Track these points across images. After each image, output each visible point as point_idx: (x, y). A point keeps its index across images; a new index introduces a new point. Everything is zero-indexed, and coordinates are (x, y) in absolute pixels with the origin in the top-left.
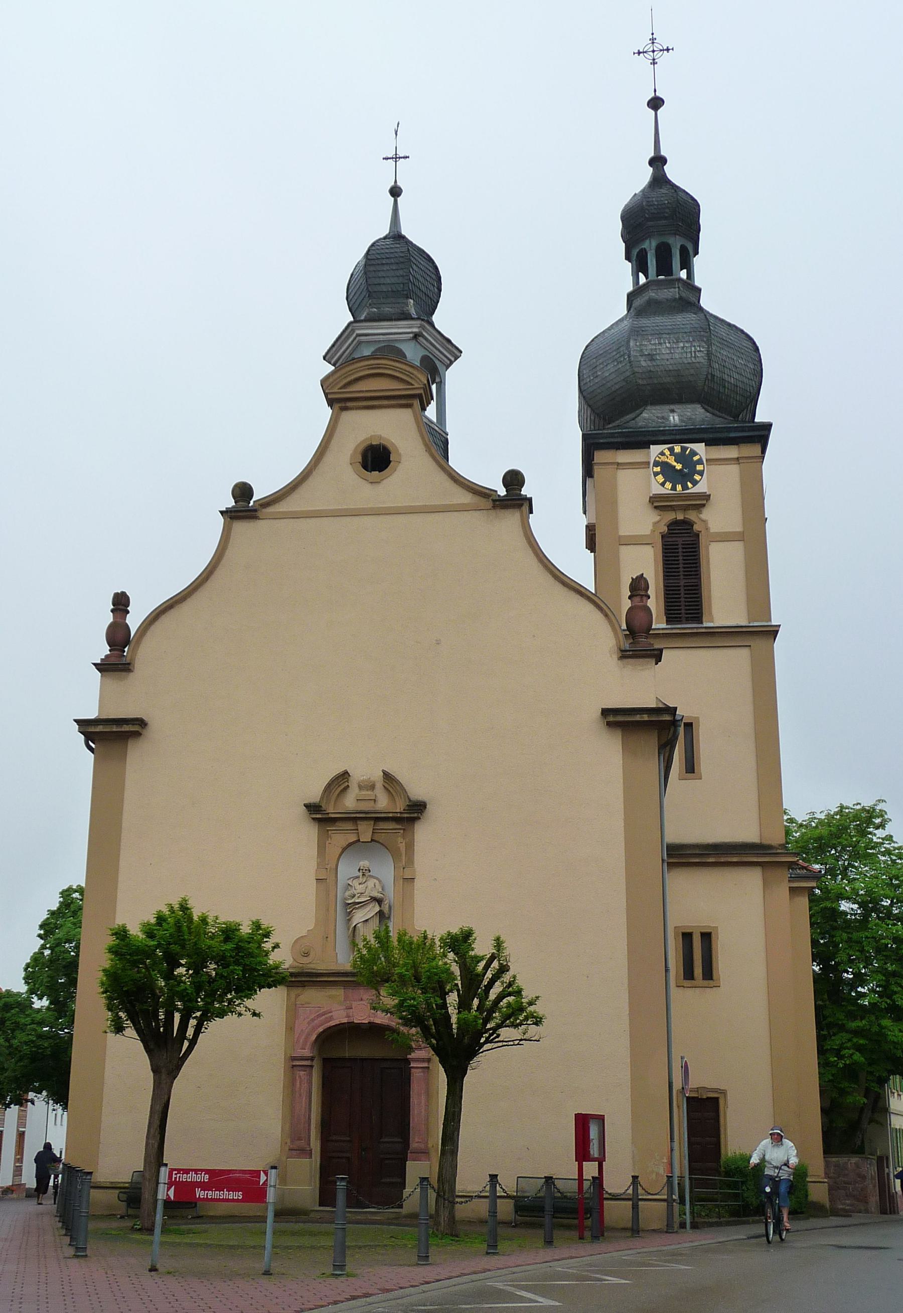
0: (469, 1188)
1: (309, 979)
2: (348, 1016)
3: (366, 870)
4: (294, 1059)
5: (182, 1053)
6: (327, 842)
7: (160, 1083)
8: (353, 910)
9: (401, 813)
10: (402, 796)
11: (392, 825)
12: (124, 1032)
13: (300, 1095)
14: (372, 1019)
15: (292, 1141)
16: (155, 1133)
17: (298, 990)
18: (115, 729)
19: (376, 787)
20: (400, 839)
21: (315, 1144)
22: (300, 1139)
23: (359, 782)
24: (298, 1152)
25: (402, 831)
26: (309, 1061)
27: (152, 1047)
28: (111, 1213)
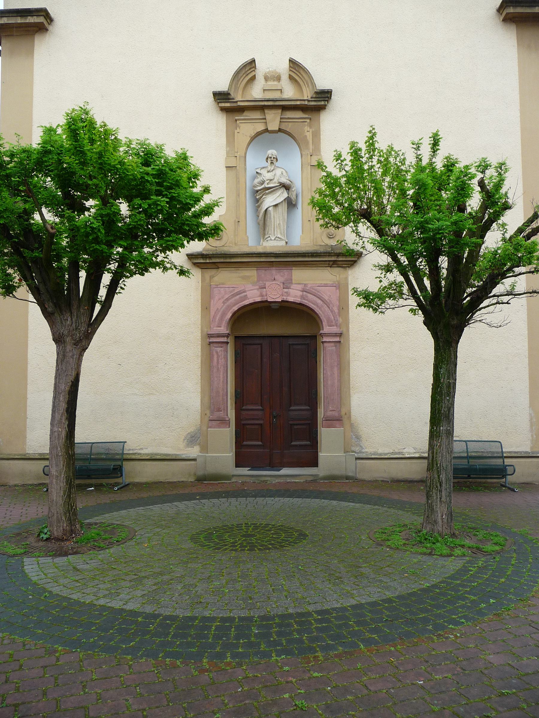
0: (380, 451)
1: (222, 260)
2: (261, 295)
3: (274, 158)
4: (210, 336)
5: (93, 319)
6: (236, 131)
7: (64, 356)
8: (263, 195)
9: (308, 101)
10: (310, 84)
11: (299, 114)
12: (14, 293)
13: (218, 369)
14: (285, 298)
15: (212, 412)
16: (61, 419)
17: (213, 272)
18: (19, 20)
19: (282, 79)
20: (307, 128)
21: (231, 414)
22: (219, 410)
23: (266, 73)
24: (218, 422)
25: (308, 121)
26: (226, 338)
27: (50, 310)
28: (41, 482)
